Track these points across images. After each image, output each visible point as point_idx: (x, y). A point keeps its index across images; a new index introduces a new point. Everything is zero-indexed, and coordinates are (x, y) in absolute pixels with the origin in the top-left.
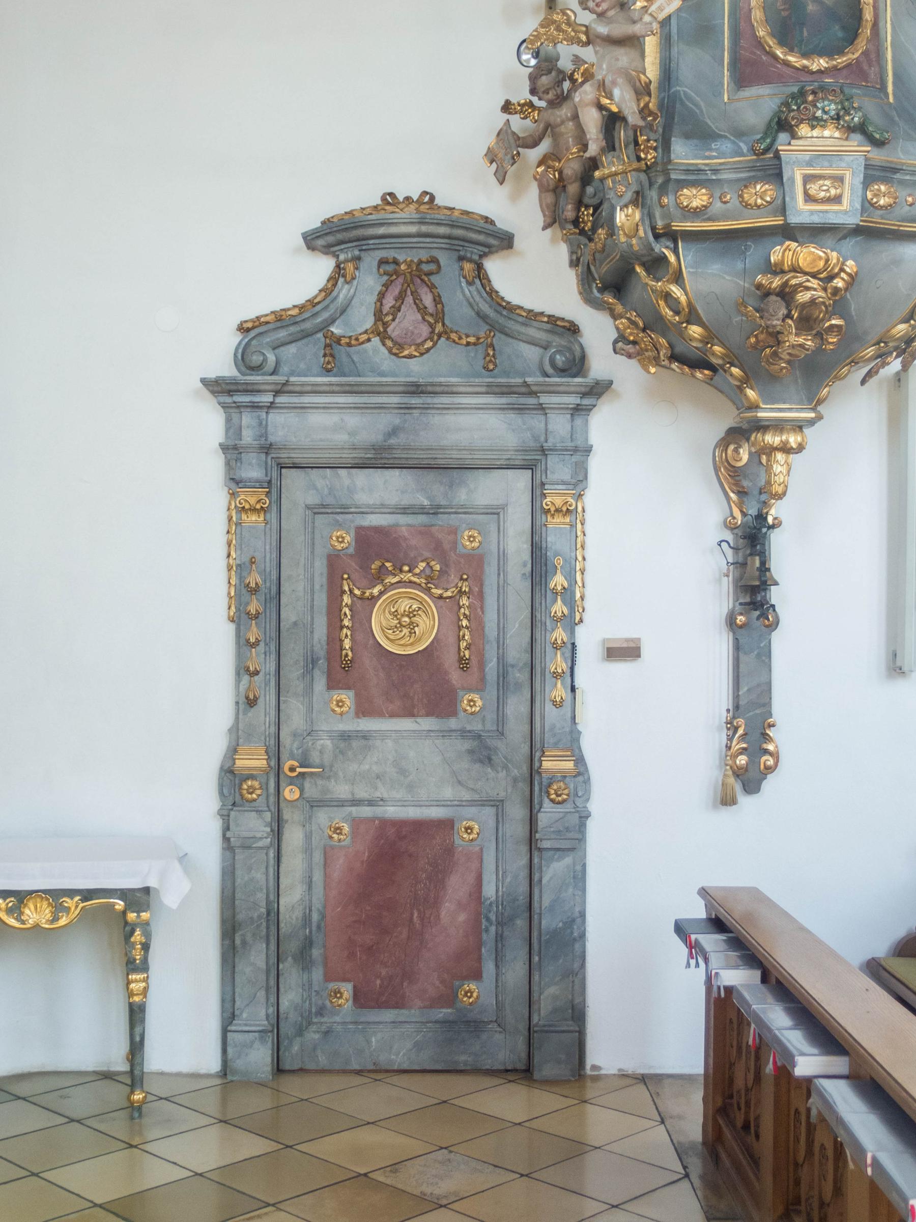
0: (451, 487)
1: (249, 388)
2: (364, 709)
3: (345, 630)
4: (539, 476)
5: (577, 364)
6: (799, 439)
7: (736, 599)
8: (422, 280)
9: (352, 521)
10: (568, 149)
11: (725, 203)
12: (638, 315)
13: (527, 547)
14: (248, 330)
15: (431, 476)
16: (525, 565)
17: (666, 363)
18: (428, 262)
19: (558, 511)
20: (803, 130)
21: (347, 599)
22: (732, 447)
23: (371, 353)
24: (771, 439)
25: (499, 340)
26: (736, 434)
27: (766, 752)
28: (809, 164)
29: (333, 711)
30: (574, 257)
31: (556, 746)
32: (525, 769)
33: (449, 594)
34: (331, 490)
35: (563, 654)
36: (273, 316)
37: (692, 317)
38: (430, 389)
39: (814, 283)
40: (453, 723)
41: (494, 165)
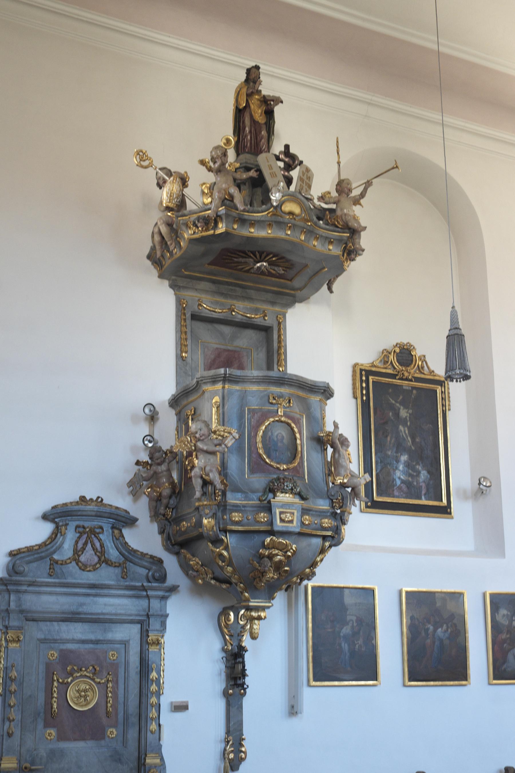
1: (17, 583)
2: (61, 737)
3: (54, 699)
5: (163, 578)
6: (265, 614)
8: (95, 536)
11: (248, 520)
13: (138, 659)
14: (15, 555)
15: (96, 626)
16: (137, 668)
18: (98, 528)
19: (154, 643)
21: (55, 684)
27: (242, 751)
28: (282, 507)
29: (47, 738)
30: (162, 530)
31: (152, 752)
32: (136, 764)
33: (103, 681)
35: (155, 709)
36: (26, 549)
40: (103, 742)
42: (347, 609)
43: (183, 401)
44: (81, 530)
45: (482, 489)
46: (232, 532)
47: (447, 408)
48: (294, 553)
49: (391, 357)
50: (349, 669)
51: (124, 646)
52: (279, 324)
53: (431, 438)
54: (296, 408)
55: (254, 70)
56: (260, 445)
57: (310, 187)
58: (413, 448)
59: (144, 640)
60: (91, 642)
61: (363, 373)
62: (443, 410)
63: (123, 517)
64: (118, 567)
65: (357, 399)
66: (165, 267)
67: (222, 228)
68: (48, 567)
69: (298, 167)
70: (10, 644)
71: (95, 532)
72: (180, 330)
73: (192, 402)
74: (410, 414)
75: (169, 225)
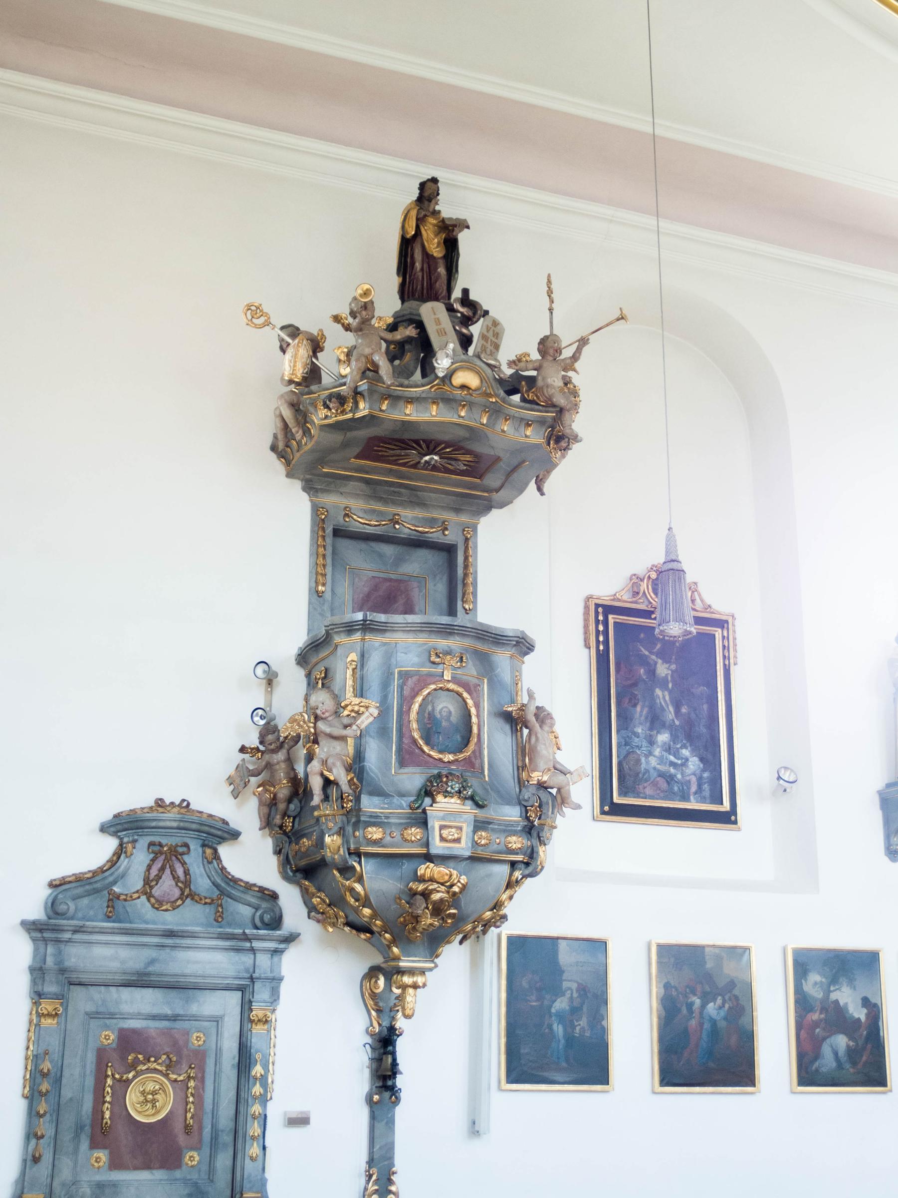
0: (187, 1002)
2: (116, 1164)
3: (107, 1105)
4: (247, 996)
5: (276, 922)
6: (424, 980)
7: (372, 1085)
8: (177, 858)
9: (116, 1024)
10: (280, 780)
12: (326, 896)
13: (235, 1046)
14: (56, 886)
15: (173, 994)
16: (234, 1058)
17: (342, 927)
19: (259, 1021)
20: (440, 798)
21: (109, 1081)
22: (373, 980)
23: (139, 906)
24: (407, 980)
25: (226, 901)
26: (373, 972)
28: (443, 819)
29: (93, 1165)
33: (181, 1078)
34: (104, 1001)
35: (258, 1122)
37: (367, 903)
38: (180, 934)
39: (443, 888)
40: (178, 1174)
41: (232, 787)
42: (563, 972)
43: (314, 654)
44: (157, 848)
45: (784, 783)
46: (369, 855)
47: (732, 661)
48: (464, 887)
49: (644, 586)
50: (564, 1064)
51: (215, 1023)
52: (467, 540)
53: (705, 707)
54: (471, 670)
55: (429, 184)
56: (414, 725)
57: (497, 347)
58: (677, 723)
59: (246, 1015)
60: (166, 1018)
61: (600, 610)
62: (725, 665)
63: (219, 830)
64: (210, 904)
65: (590, 648)
66: (293, 462)
67: (364, 408)
68: (106, 904)
69: (482, 319)
70: (43, 1020)
71: (176, 851)
72: (315, 551)
73: (323, 659)
74: (672, 671)
75: (295, 406)
